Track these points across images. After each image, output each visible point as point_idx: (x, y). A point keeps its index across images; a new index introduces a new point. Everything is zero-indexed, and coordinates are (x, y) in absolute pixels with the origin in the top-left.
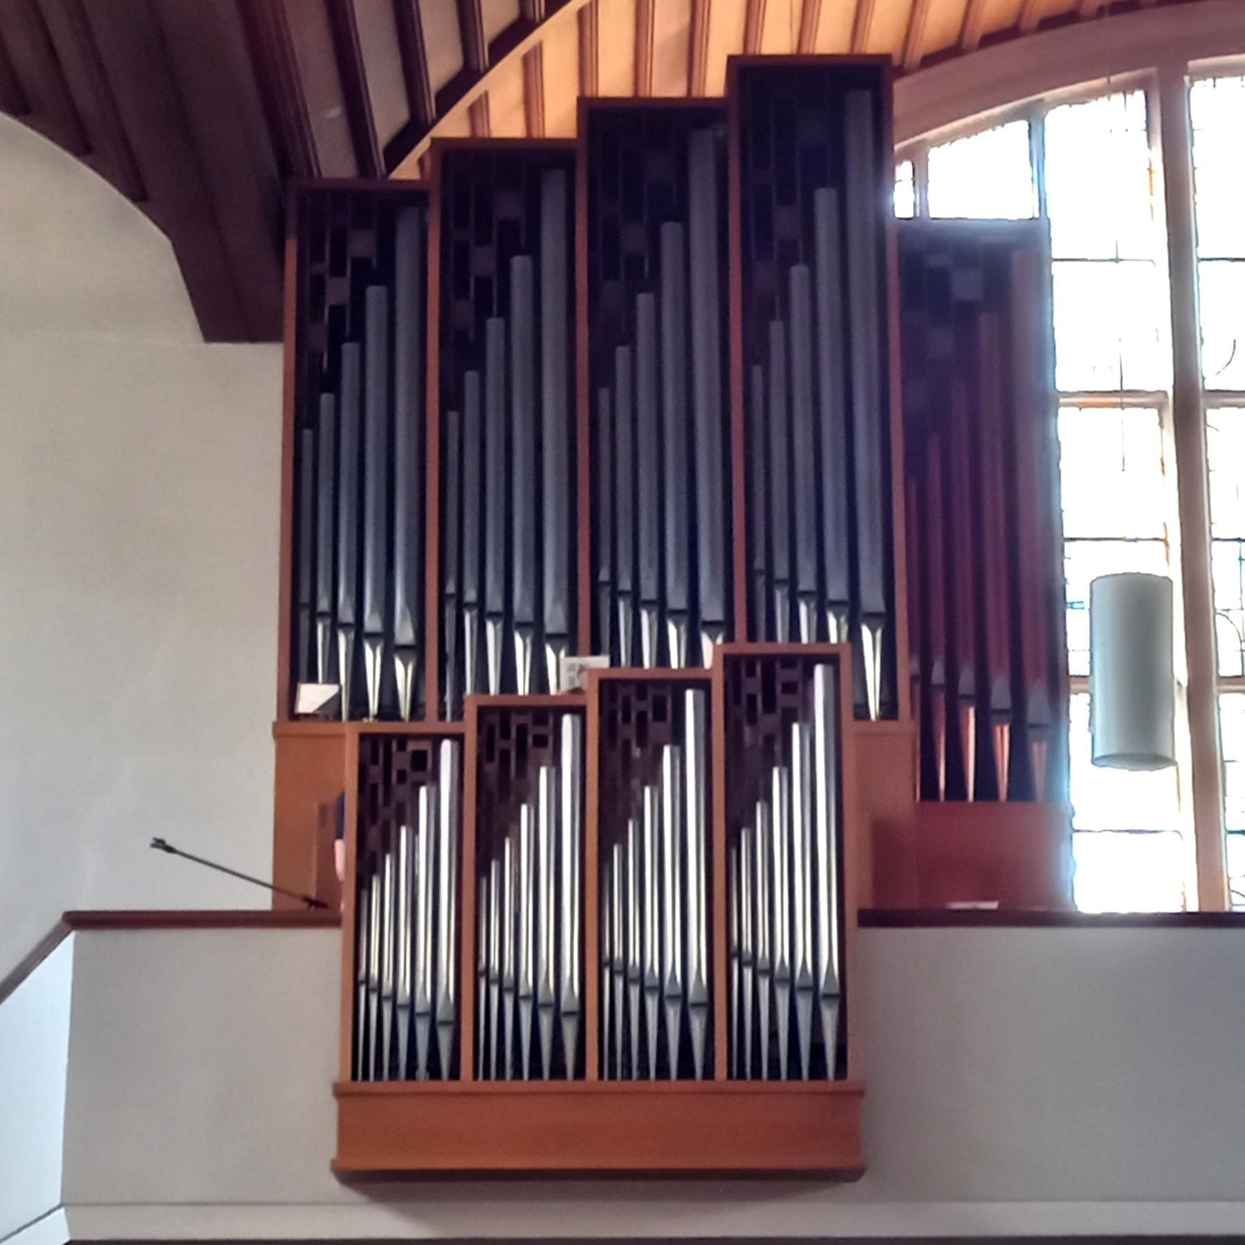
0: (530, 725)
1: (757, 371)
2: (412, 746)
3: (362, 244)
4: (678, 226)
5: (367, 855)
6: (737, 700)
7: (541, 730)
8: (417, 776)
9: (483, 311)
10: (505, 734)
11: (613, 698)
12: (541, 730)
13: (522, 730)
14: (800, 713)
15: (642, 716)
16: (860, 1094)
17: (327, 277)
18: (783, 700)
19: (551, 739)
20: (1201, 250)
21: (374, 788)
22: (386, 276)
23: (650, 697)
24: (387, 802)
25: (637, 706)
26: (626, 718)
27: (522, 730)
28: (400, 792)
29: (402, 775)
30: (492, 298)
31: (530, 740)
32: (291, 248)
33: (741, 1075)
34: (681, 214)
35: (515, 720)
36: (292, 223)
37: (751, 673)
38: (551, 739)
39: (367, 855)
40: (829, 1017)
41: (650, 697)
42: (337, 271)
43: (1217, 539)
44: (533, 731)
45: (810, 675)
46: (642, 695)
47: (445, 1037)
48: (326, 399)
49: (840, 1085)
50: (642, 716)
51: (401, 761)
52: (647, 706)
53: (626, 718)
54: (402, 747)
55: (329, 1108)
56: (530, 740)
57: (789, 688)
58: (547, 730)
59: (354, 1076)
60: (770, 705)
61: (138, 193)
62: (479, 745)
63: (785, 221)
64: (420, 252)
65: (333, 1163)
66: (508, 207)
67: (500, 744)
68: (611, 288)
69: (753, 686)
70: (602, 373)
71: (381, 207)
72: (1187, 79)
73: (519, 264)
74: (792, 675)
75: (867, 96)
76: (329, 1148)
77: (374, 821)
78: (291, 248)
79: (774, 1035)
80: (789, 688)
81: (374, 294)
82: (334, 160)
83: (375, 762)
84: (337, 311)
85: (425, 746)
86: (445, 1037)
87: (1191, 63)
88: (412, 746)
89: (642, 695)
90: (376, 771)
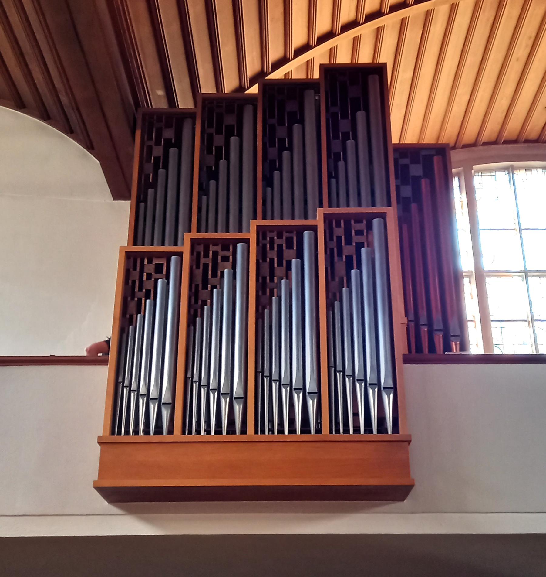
0: (220, 251)
1: (334, 181)
2: (156, 261)
3: (168, 134)
4: (300, 126)
5: (128, 316)
6: (331, 239)
7: (226, 253)
8: (158, 276)
9: (218, 157)
10: (206, 256)
11: (264, 238)
12: (226, 253)
13: (215, 254)
14: (366, 244)
15: (280, 247)
16: (409, 442)
17: (153, 146)
18: (356, 239)
19: (231, 258)
20: (481, 227)
21: (134, 282)
22: (178, 145)
23: (284, 238)
24: (140, 289)
25: (277, 241)
26: (272, 248)
27: (215, 254)
28: (148, 285)
29: (149, 276)
30: (222, 153)
31: (219, 257)
32: (138, 133)
33: (338, 431)
34: (302, 122)
35: (212, 249)
36: (139, 122)
37: (338, 225)
38: (231, 258)
39: (128, 316)
40: (388, 401)
41: (284, 238)
42: (158, 143)
43: (492, 321)
44: (222, 253)
45: (369, 227)
46: (280, 236)
47: (165, 414)
48: (151, 191)
49: (396, 437)
50: (280, 247)
51: (149, 268)
52: (283, 242)
53: (272, 248)
54: (150, 262)
55: (95, 451)
56: (219, 257)
57: (359, 233)
58: (229, 254)
59: (113, 433)
60: (349, 242)
61: (90, 147)
62: (191, 260)
63: (344, 125)
64: (252, 129)
65: (95, 482)
66: (230, 120)
67: (203, 260)
68: (273, 152)
69: (339, 232)
70: (268, 182)
71: (176, 119)
72: (473, 171)
73: (234, 140)
74: (362, 226)
75: (377, 77)
76: (95, 476)
77: (133, 299)
78: (138, 133)
79: (356, 414)
80: (359, 233)
81: (173, 151)
82: (157, 99)
83: (135, 269)
84: (157, 159)
85: (163, 261)
86: (165, 414)
87: (474, 166)
88: (156, 261)
89: (280, 236)
90: (135, 275)
